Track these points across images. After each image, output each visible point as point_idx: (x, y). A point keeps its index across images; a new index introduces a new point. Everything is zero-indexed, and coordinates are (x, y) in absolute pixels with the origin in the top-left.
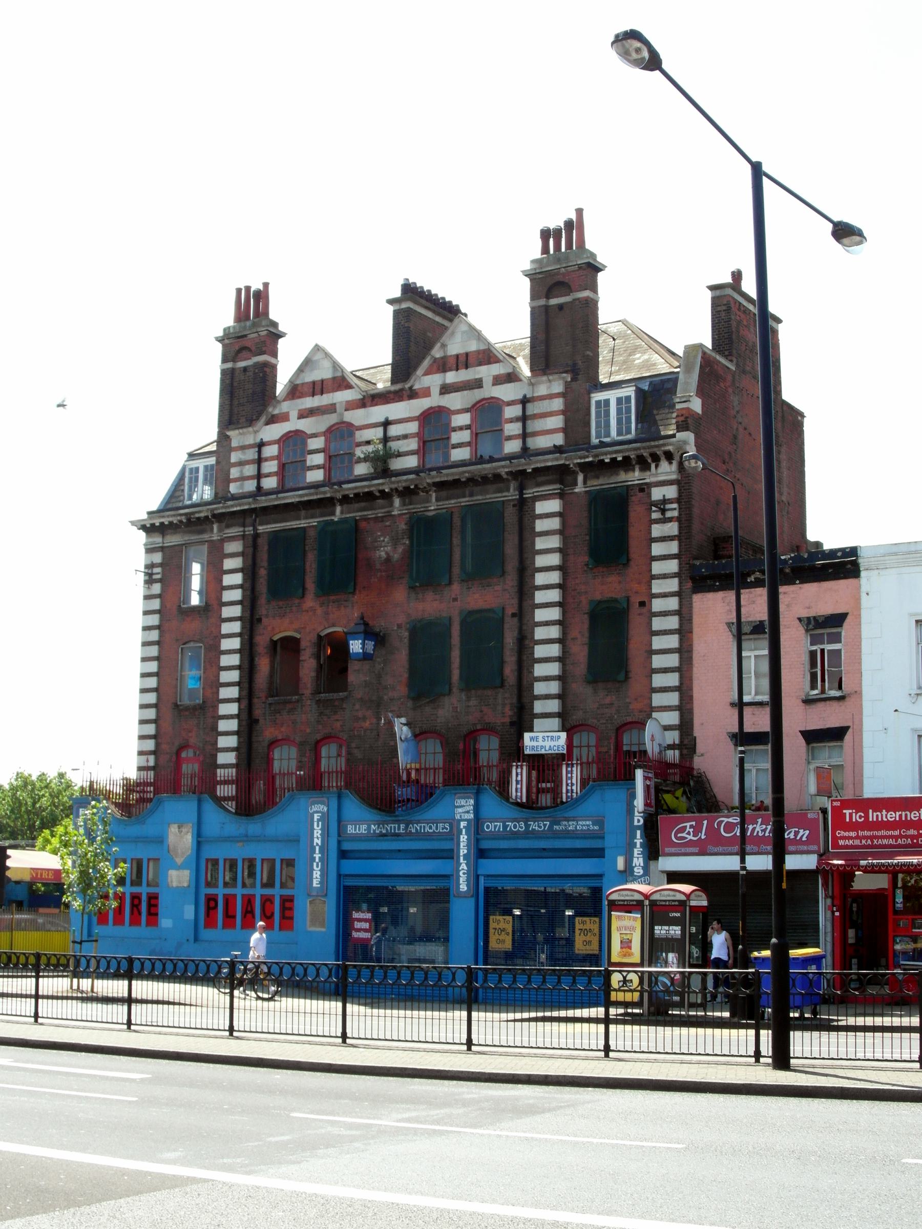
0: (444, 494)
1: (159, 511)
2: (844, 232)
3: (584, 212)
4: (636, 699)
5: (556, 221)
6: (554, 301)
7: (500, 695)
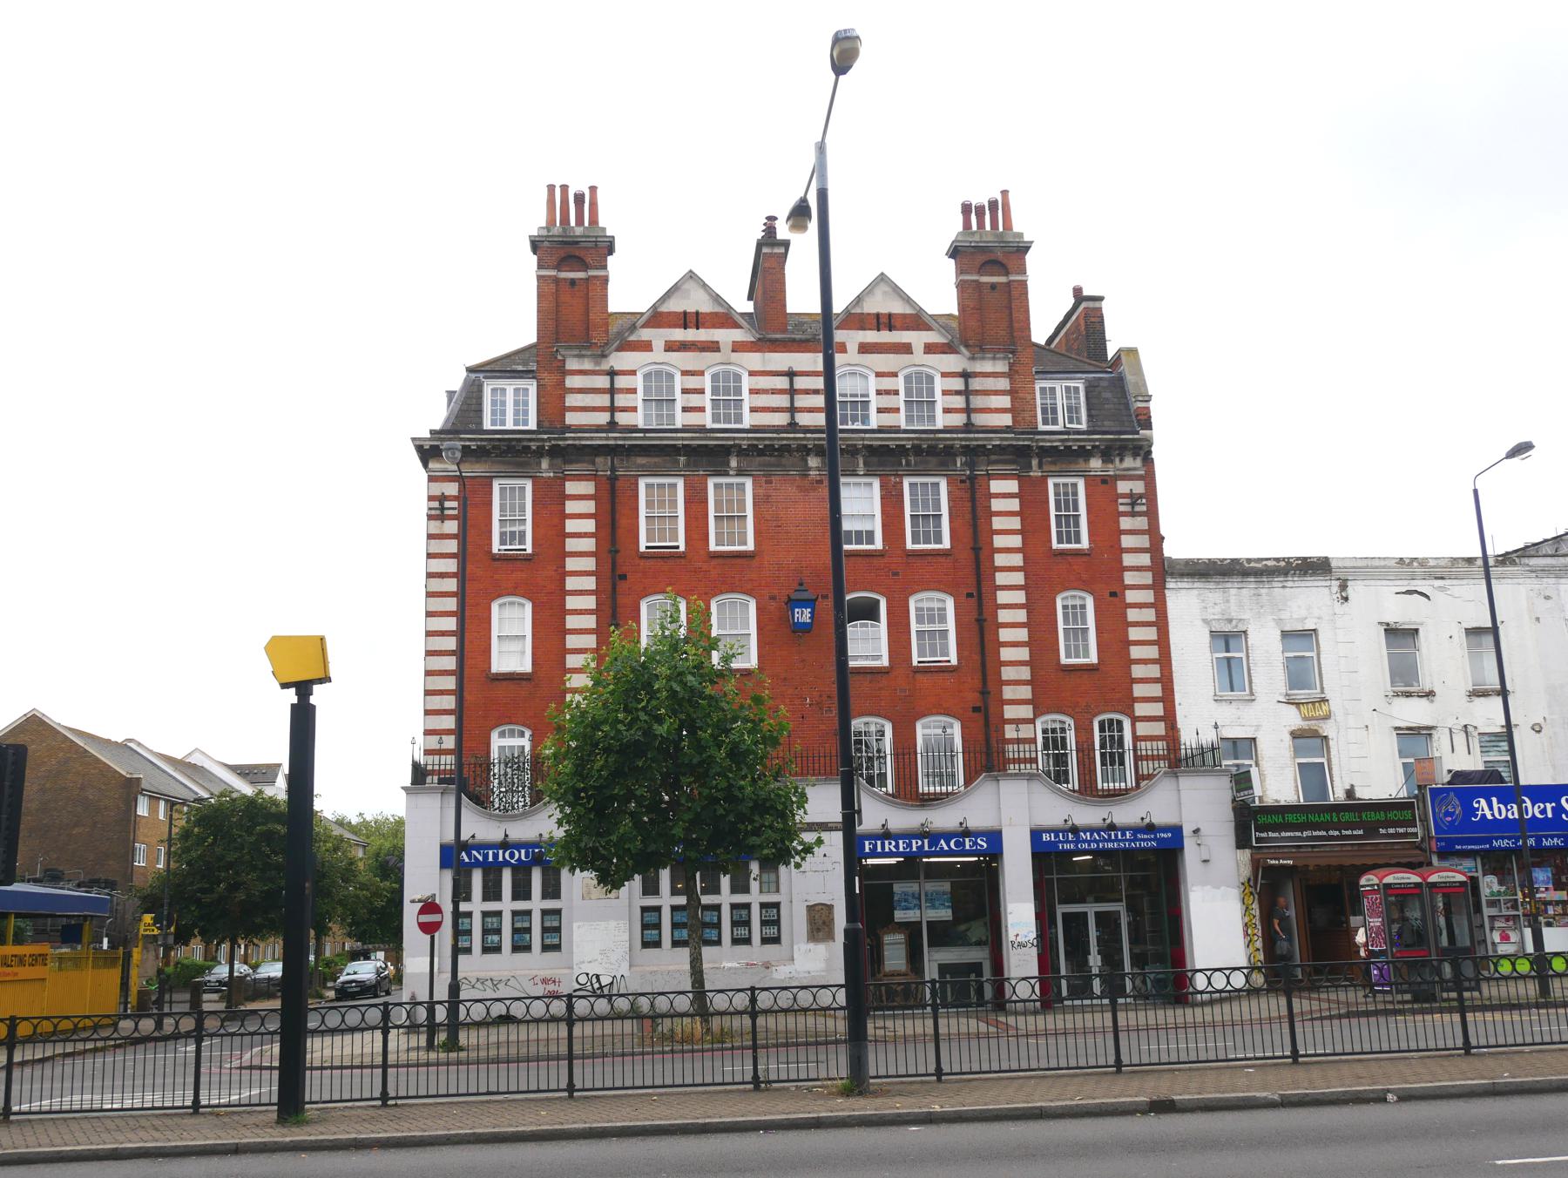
0: (875, 459)
1: (441, 432)
2: (844, 54)
5: (980, 198)
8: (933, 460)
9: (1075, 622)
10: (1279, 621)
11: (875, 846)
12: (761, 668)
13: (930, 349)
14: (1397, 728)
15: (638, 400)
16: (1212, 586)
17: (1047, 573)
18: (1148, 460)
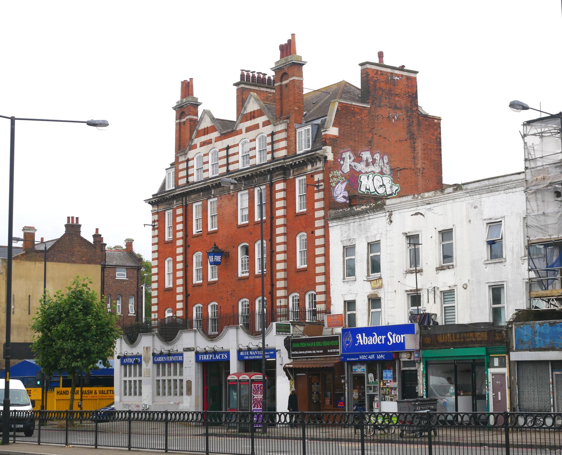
3: (296, 36)
6: (284, 83)
10: (367, 237)
14: (406, 291)
15: (239, 157)
16: (344, 223)
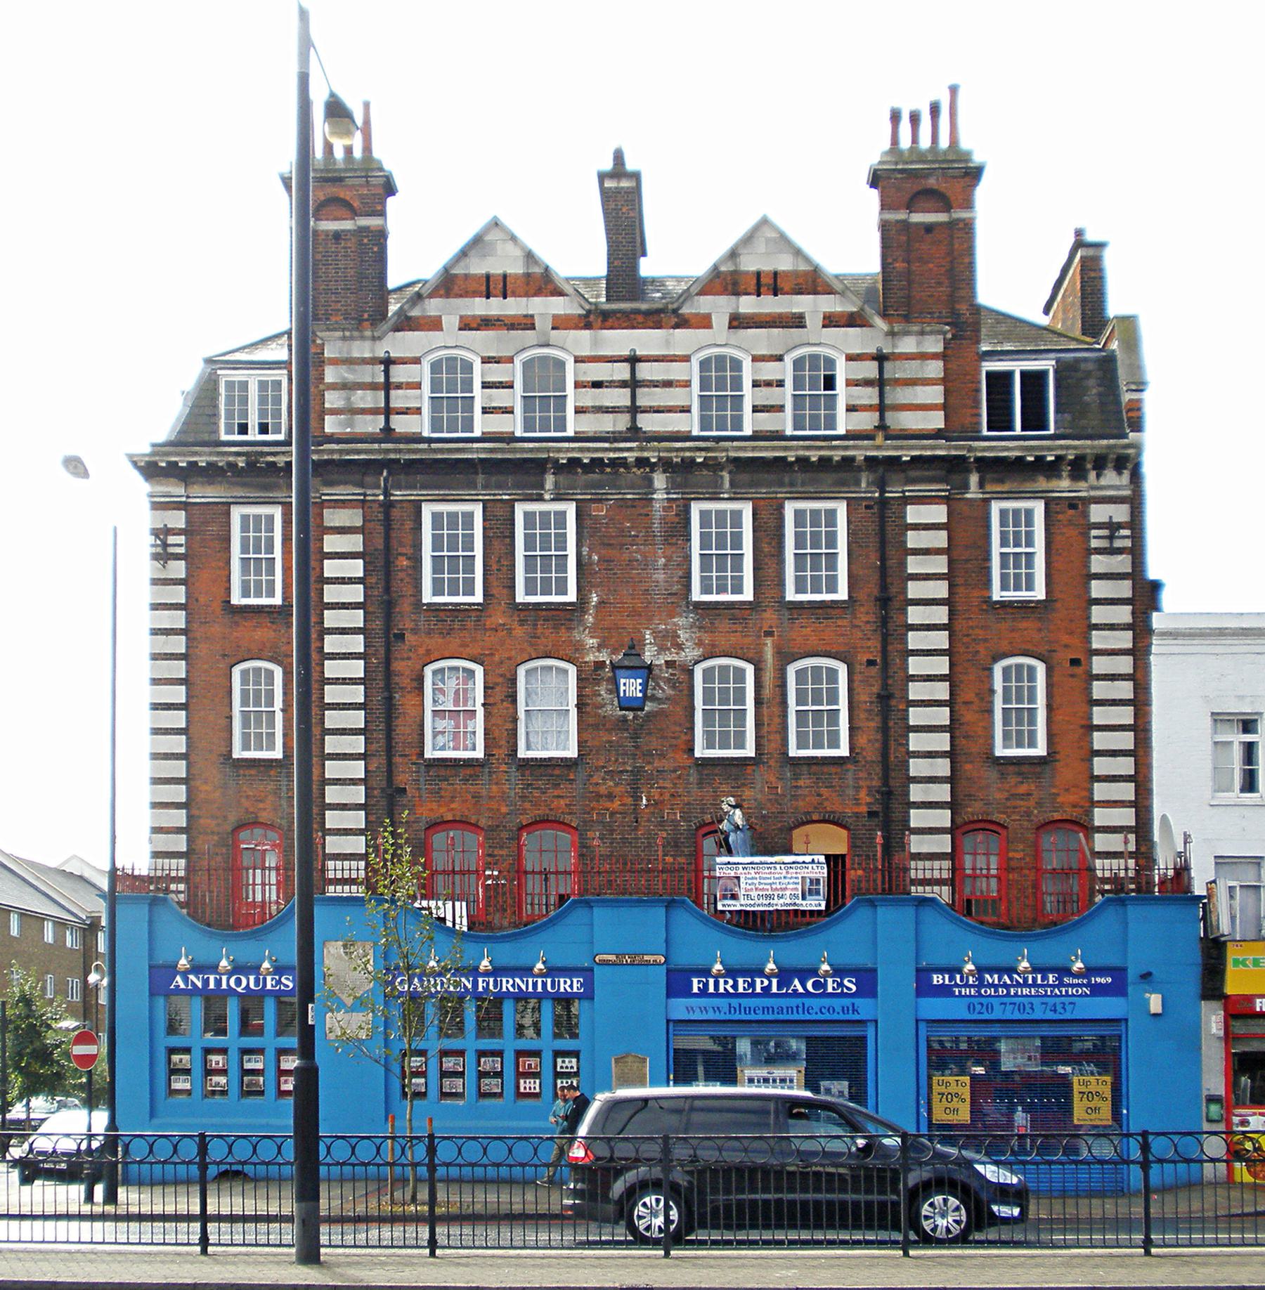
0: (745, 477)
1: (169, 444)
4: (1067, 790)
7: (850, 775)
8: (830, 477)
9: (257, 703)
11: (706, 985)
12: (425, 760)
13: (830, 321)
17: (980, 628)
18: (1136, 478)
